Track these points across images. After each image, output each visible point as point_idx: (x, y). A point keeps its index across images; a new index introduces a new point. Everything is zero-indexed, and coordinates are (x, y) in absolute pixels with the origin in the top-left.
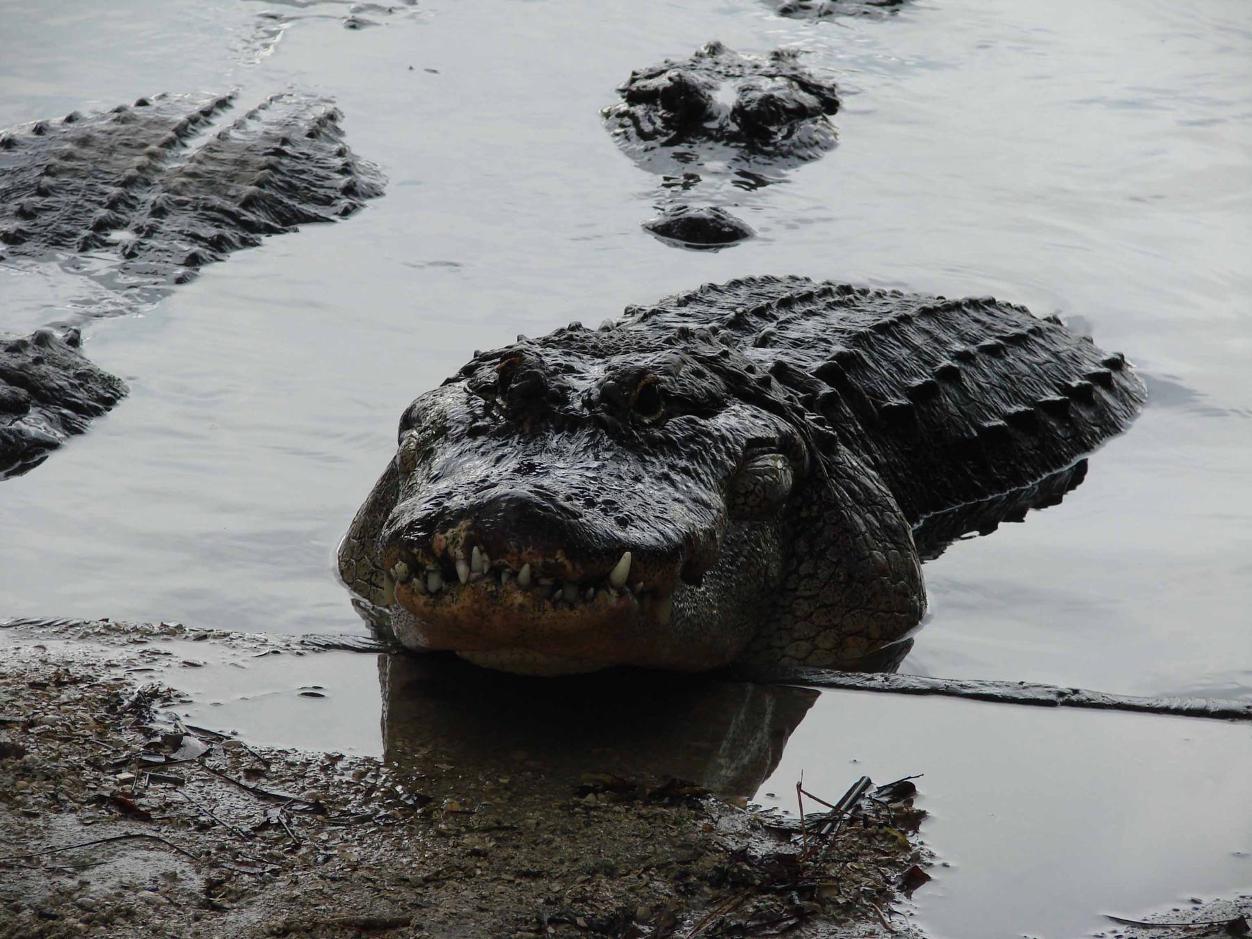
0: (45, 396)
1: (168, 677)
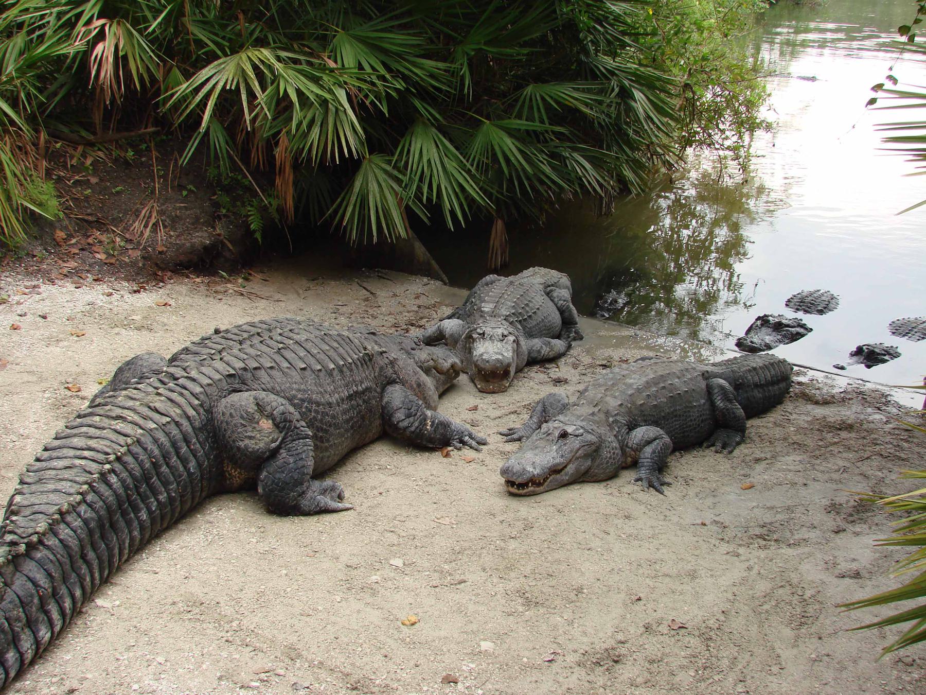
0: (889, 354)
1: (892, 393)
